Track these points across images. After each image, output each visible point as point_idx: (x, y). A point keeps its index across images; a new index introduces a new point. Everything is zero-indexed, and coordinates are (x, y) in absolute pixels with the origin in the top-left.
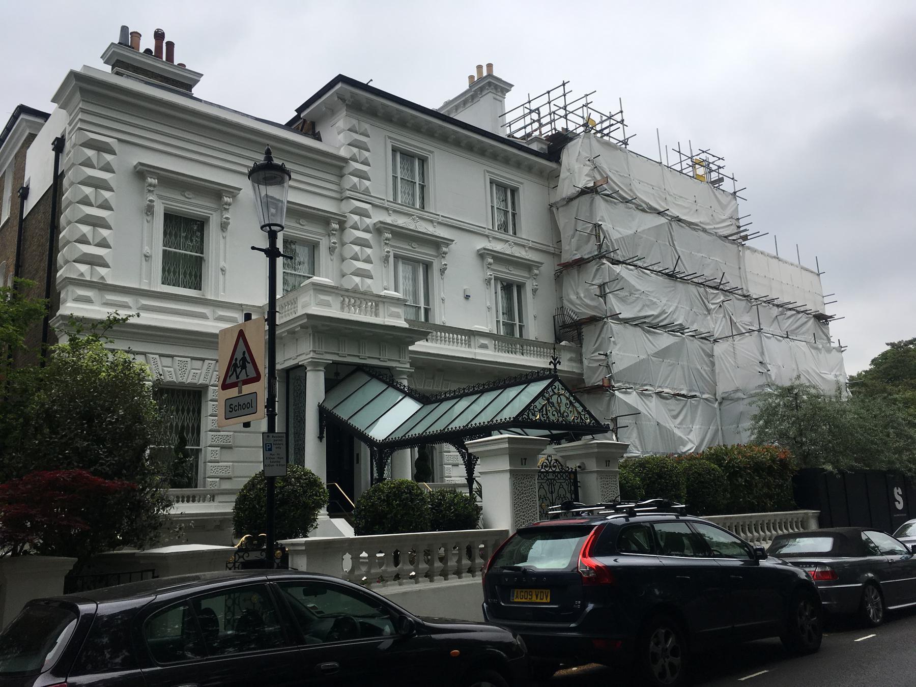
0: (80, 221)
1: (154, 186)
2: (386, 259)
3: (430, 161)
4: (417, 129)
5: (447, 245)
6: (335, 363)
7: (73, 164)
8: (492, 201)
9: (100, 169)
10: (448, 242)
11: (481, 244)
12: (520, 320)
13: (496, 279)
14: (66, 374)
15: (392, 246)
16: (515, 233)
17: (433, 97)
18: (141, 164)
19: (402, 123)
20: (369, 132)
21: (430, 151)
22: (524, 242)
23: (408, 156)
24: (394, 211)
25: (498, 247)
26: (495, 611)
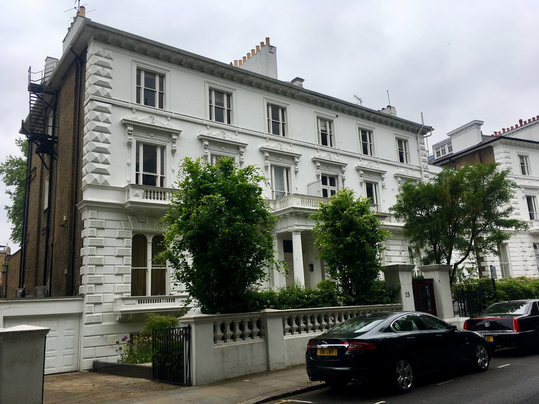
1: (131, 131)
2: (266, 167)
3: (234, 94)
7: (90, 120)
8: (268, 117)
9: (104, 122)
11: (358, 163)
13: (364, 181)
14: (319, 241)
15: (209, 149)
16: (331, 146)
18: (124, 120)
21: (233, 89)
22: (337, 151)
23: (219, 93)
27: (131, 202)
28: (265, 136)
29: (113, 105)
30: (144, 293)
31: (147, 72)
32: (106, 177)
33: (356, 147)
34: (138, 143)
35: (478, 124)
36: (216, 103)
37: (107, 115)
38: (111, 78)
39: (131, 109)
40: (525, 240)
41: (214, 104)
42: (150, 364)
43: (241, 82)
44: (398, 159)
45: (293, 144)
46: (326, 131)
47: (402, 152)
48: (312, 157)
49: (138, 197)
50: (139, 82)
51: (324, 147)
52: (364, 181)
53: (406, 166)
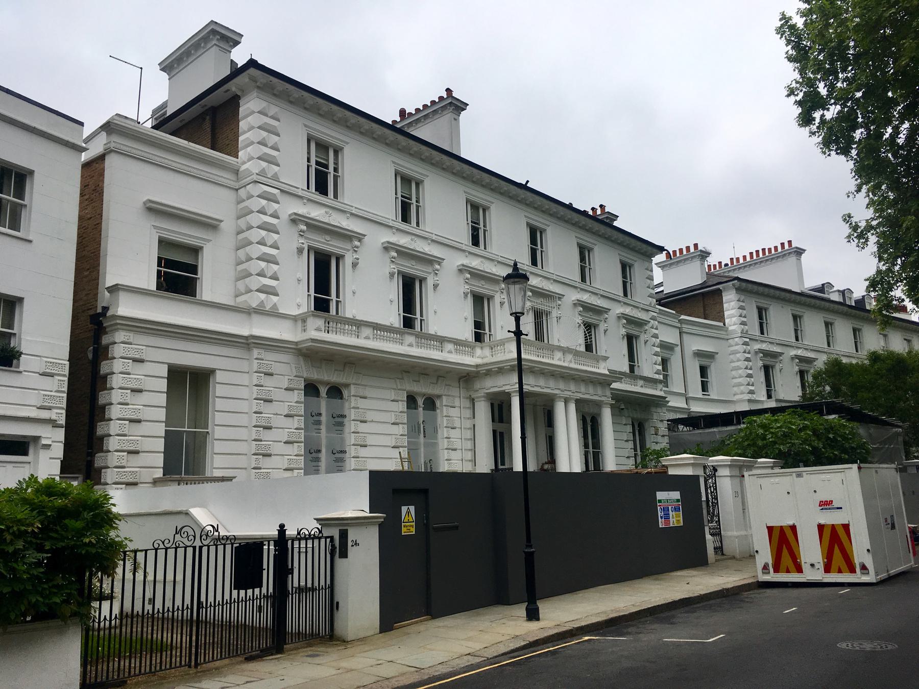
5: (560, 299)
10: (360, 237)
12: (421, 315)
15: (306, 238)
16: (485, 248)
22: (347, 208)
23: (323, 147)
27: (313, 340)
28: (300, 193)
32: (275, 299)
35: (704, 255)
36: (317, 163)
38: (278, 150)
39: (576, 287)
40: (276, 368)
41: (399, 195)
42: (660, 495)
44: (578, 278)
46: (326, 167)
47: (326, 174)
48: (290, 215)
49: (316, 331)
51: (474, 250)
52: (399, 272)
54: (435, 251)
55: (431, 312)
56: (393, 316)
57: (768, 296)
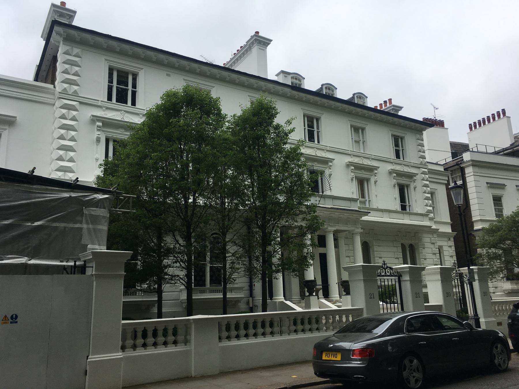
0: (59, 149)
4: (202, 75)
6: (335, 230)
10: (331, 160)
11: (390, 167)
17: (221, 58)
19: (192, 72)
20: (80, 54)
22: (323, 148)
24: (395, 163)
25: (398, 168)
26: (318, 373)
29: (81, 103)
30: (204, 285)
31: (119, 72)
33: (389, 152)
34: (107, 141)
37: (74, 113)
43: (147, 60)
45: (372, 159)
47: (313, 131)
48: (389, 169)
50: (111, 81)
51: (398, 161)
53: (318, 146)
54: (330, 155)
55: (374, 196)
56: (397, 205)
57: (323, 107)
